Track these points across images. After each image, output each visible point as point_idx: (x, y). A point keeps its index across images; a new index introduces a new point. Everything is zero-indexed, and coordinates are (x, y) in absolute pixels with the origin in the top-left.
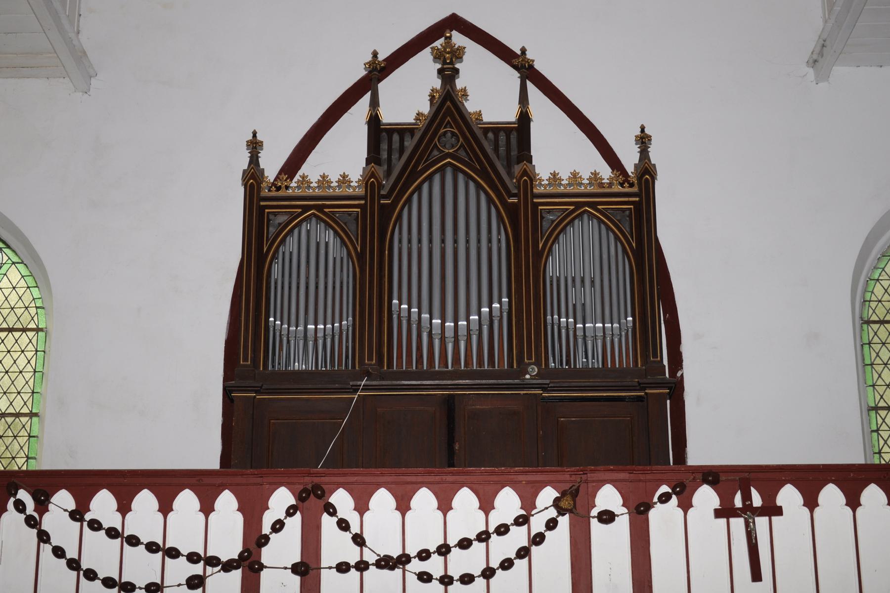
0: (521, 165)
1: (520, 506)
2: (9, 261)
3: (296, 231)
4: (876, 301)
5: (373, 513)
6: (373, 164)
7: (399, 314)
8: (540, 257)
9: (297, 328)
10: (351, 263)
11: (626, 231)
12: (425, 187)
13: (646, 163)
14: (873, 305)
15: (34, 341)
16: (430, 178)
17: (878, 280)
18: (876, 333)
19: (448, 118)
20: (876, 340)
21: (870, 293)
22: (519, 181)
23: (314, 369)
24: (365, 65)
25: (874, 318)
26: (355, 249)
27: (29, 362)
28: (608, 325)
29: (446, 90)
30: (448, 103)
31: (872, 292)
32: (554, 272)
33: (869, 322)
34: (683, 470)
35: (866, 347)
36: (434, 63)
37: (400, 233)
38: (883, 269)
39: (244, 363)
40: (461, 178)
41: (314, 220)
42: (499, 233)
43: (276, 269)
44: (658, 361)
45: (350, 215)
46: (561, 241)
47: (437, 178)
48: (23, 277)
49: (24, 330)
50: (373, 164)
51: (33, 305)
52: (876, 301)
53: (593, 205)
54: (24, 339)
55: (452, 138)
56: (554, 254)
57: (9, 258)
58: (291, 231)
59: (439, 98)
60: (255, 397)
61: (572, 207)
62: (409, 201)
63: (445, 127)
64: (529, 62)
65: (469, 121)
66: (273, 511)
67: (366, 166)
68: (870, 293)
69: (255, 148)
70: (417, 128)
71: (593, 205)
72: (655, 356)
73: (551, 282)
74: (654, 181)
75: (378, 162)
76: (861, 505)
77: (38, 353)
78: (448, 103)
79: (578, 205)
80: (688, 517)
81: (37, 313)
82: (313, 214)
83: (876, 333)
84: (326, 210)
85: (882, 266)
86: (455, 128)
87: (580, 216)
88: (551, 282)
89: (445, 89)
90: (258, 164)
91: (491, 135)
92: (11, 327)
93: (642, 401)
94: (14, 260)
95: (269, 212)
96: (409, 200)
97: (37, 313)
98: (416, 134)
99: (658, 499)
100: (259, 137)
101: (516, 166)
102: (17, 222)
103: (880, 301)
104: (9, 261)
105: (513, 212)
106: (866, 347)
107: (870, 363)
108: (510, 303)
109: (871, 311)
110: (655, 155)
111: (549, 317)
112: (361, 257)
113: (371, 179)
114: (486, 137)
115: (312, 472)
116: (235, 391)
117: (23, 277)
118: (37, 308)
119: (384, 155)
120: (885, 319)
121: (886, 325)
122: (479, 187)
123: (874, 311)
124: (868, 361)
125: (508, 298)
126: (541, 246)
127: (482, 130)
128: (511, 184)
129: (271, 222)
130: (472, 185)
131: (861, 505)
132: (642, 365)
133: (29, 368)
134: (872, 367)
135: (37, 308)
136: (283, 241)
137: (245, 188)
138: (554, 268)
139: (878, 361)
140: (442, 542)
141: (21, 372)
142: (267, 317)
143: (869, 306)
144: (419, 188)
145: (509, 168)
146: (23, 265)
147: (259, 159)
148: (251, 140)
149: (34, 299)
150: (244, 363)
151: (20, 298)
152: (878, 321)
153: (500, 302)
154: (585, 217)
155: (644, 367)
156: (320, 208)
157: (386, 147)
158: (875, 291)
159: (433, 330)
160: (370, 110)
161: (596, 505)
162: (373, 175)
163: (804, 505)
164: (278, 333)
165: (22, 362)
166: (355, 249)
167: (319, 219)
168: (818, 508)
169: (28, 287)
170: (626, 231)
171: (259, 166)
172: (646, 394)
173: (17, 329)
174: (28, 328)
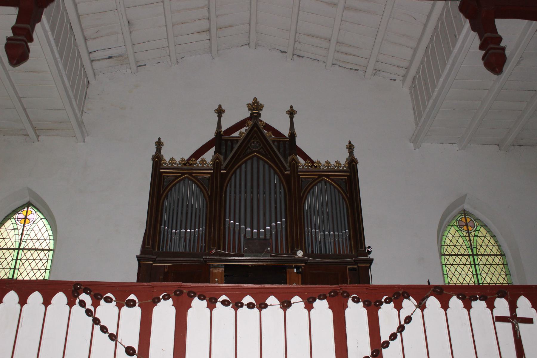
0: (291, 156)
1: (304, 307)
2: (39, 218)
3: (178, 185)
4: (447, 245)
5: (218, 309)
6: (218, 153)
7: (229, 226)
8: (301, 199)
9: (176, 231)
10: (205, 200)
11: (344, 189)
12: (243, 166)
13: (353, 157)
14: (446, 247)
15: (47, 255)
16: (246, 162)
17: (447, 236)
18: (448, 260)
19: (255, 135)
20: (448, 263)
21: (444, 242)
22: (290, 164)
23: (184, 251)
24: (215, 111)
25: (447, 253)
26: (208, 194)
27: (44, 265)
28: (336, 233)
29: (255, 122)
30: (255, 128)
31: (445, 241)
32: (308, 208)
33: (444, 255)
34: (396, 287)
35: (444, 266)
36: (248, 111)
37: (230, 187)
38: (449, 231)
39: (148, 247)
40: (261, 163)
41: (187, 180)
42: (280, 189)
43: (167, 202)
44: (364, 250)
45: (205, 177)
46: (311, 193)
47: (249, 162)
48: (45, 225)
49: (43, 250)
50: (218, 153)
51: (48, 238)
52: (447, 245)
53: (327, 176)
54: (42, 254)
55: (257, 144)
56: (308, 198)
57: (39, 217)
58: (175, 185)
59: (251, 126)
60: (152, 264)
61: (317, 177)
62: (235, 172)
63: (254, 139)
64: (294, 112)
65: (266, 136)
66: (159, 307)
67: (214, 154)
68: (444, 242)
69: (159, 145)
70: (239, 139)
71: (327, 176)
72: (362, 248)
73: (307, 212)
74: (357, 165)
75: (220, 153)
76: (495, 308)
77: (48, 261)
78: (255, 128)
79: (320, 176)
80: (400, 313)
81: (50, 242)
82: (187, 177)
83: (448, 260)
84: (194, 175)
85: (457, 218)
86: (258, 139)
87: (320, 181)
88: (307, 212)
89: (254, 121)
90: (160, 152)
91: (276, 143)
92: (37, 248)
93: (356, 270)
94: (41, 218)
95: (164, 175)
96: (235, 172)
97: (50, 242)
98: (239, 142)
99: (385, 300)
100: (162, 140)
101: (288, 157)
102: (46, 201)
103: (449, 246)
104: (39, 218)
105: (287, 178)
106: (444, 266)
107: (446, 273)
108: (286, 221)
109: (445, 250)
110: (356, 155)
111: (306, 229)
112: (210, 197)
113: (217, 160)
114: (274, 144)
115: (183, 285)
116: (141, 260)
117: (45, 225)
118: (50, 240)
119: (223, 151)
120: (452, 254)
121: (452, 256)
122: (270, 166)
123: (446, 250)
124: (445, 273)
125: (285, 219)
126: (301, 195)
127: (272, 141)
128: (287, 166)
129: (165, 180)
130: (267, 166)
131: (495, 308)
132: (355, 253)
133: (43, 268)
134: (448, 275)
135: (50, 240)
136: (171, 189)
137: (153, 162)
138: (307, 206)
139: (450, 272)
140: (263, 311)
141: (39, 269)
142: (161, 225)
143: (444, 248)
144: (240, 166)
145: (285, 158)
146: (45, 220)
147: (161, 150)
148: (157, 141)
149: (49, 236)
150: (148, 247)
151: (42, 235)
152: (448, 254)
153: (281, 221)
154: (323, 182)
155: (356, 254)
156: (190, 174)
157: (224, 148)
158: (446, 241)
159: (247, 234)
160: (217, 130)
161: (348, 306)
162: (217, 158)
163: (464, 308)
164: (166, 233)
165: (40, 265)
166: (208, 194)
167: (189, 179)
168: (472, 309)
169: (47, 230)
170: (344, 189)
171: (161, 153)
172: (358, 267)
173: (40, 250)
174: (45, 249)
